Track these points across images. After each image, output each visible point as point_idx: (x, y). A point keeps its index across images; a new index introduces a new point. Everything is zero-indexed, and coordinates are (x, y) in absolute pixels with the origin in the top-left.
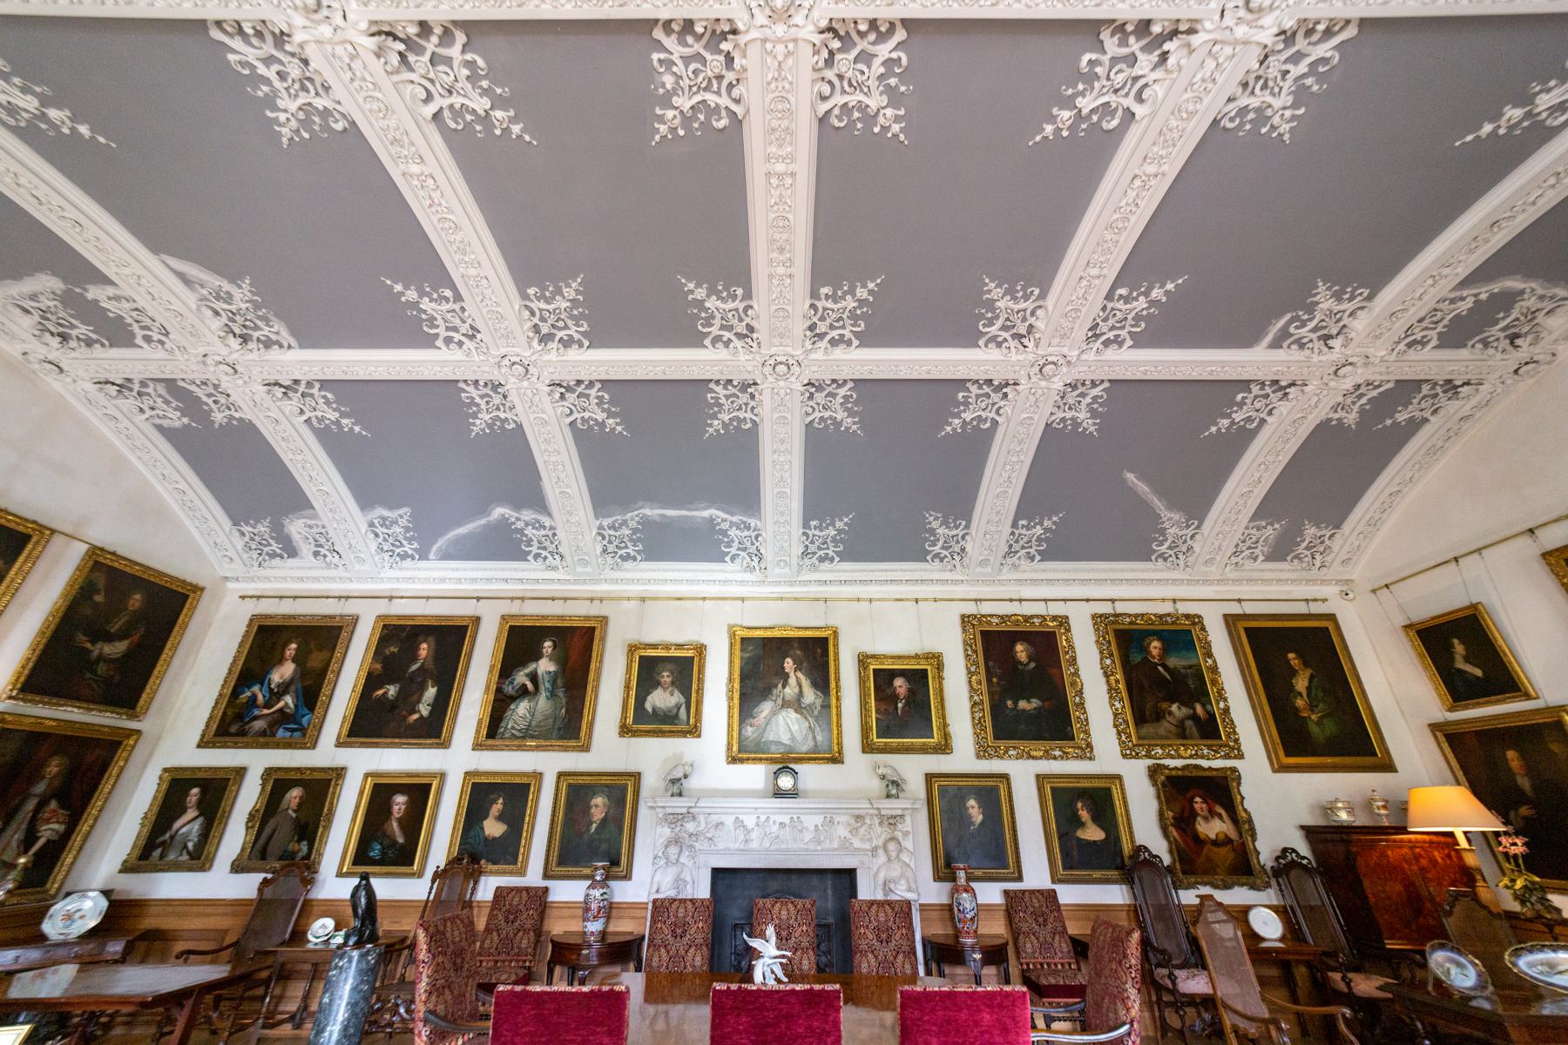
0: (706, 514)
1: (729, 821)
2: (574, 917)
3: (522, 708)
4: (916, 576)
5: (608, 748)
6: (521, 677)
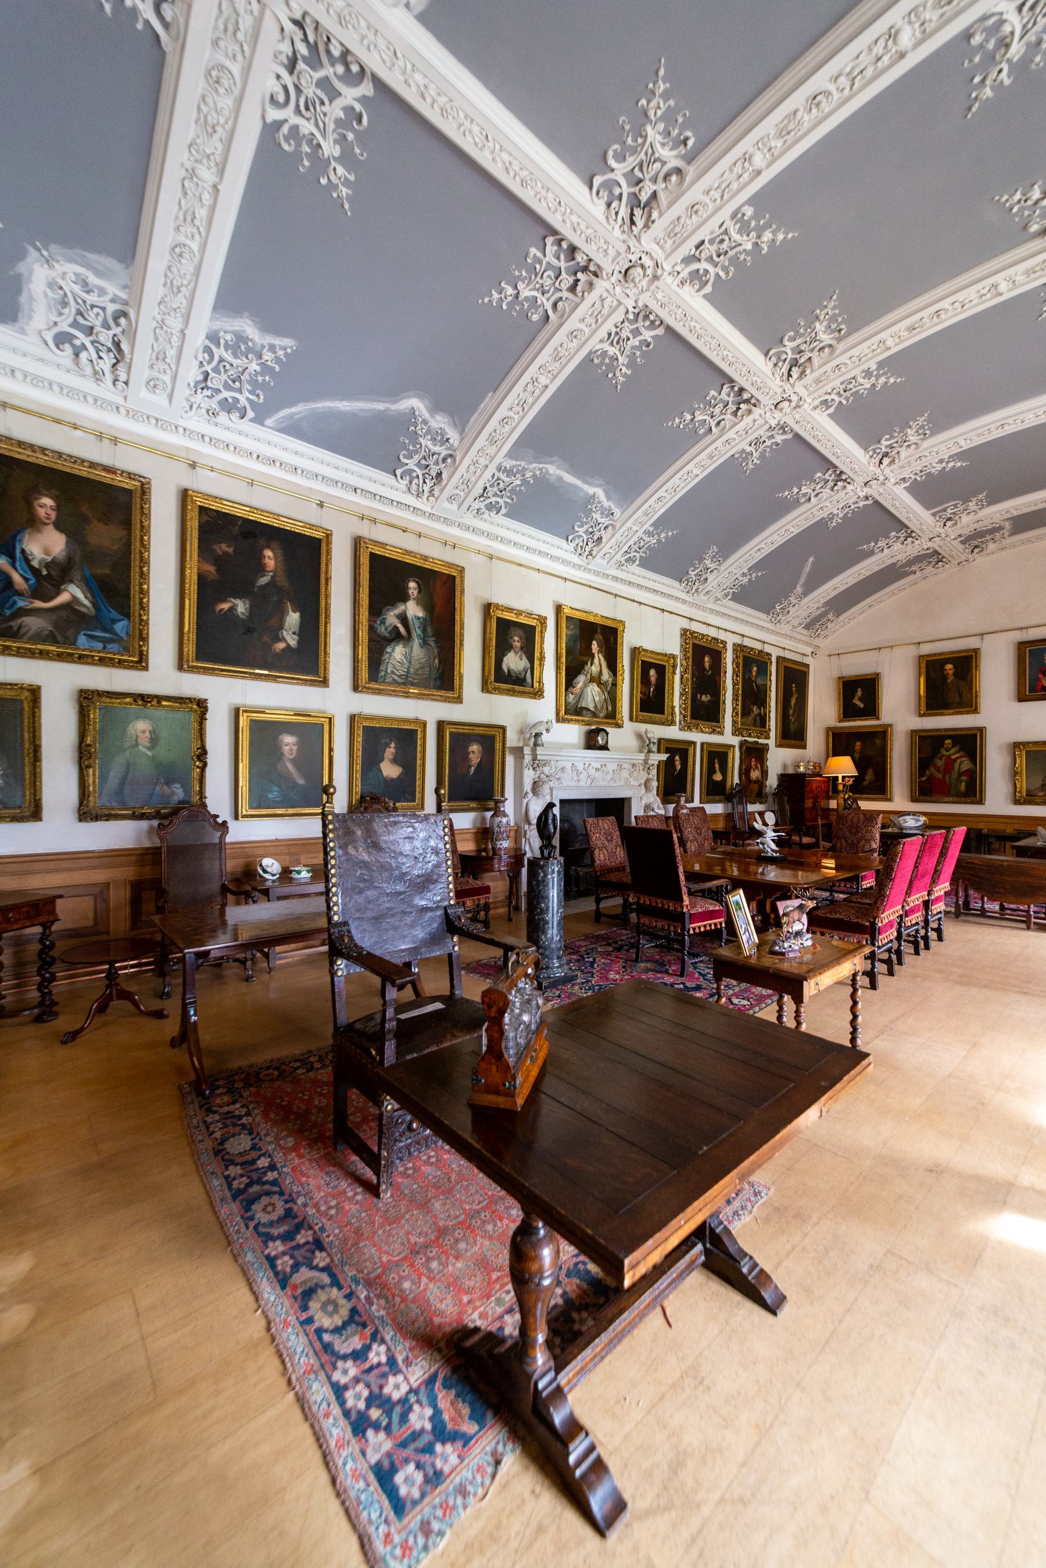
0: (591, 490)
1: (568, 765)
2: (466, 840)
3: (398, 653)
4: (665, 590)
5: (476, 705)
6: (391, 618)
